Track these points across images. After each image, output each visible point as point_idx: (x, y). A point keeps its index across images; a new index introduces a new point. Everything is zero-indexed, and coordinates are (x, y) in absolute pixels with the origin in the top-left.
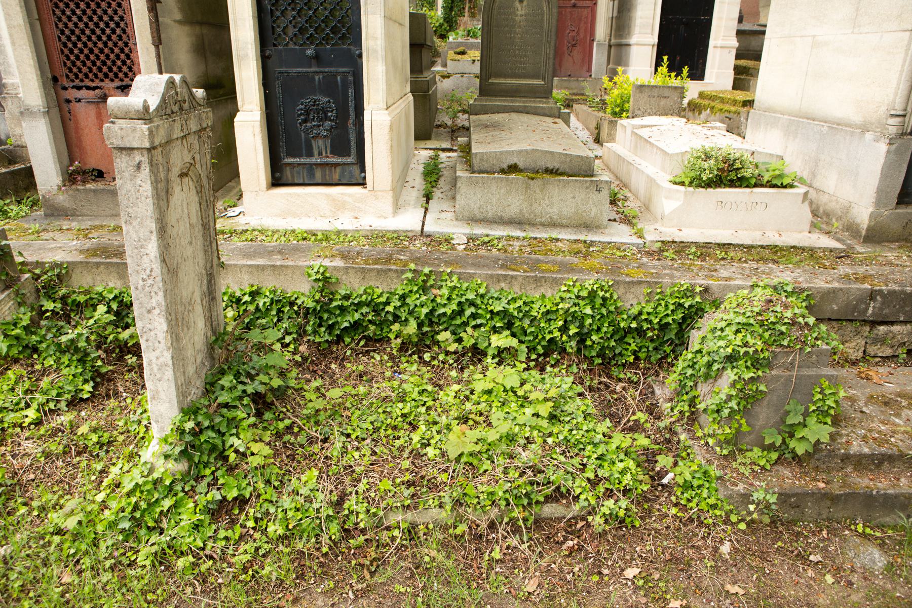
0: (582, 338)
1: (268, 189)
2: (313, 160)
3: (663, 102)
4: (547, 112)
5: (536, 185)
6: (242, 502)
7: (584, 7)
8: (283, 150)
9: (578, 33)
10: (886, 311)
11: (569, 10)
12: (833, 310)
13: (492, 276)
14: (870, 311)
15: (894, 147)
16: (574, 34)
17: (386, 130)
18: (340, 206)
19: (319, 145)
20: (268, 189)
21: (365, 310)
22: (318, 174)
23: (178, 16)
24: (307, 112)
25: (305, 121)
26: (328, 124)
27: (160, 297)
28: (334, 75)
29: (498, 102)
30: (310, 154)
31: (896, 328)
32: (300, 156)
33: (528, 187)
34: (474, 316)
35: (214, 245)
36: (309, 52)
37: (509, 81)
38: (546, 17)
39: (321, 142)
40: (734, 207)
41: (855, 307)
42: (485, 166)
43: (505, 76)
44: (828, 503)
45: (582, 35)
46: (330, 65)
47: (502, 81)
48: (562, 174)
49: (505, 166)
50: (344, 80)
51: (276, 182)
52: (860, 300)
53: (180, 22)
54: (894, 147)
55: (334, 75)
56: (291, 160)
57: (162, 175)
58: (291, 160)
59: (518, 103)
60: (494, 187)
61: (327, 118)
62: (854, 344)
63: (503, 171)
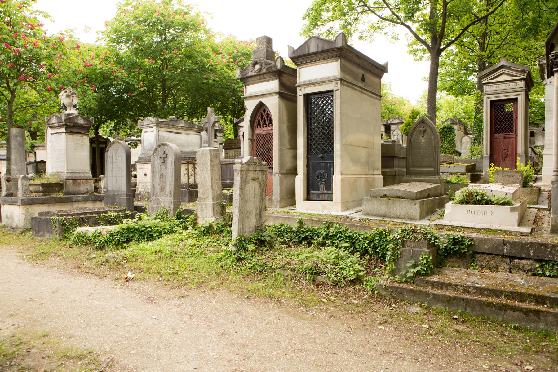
0: (375, 247)
1: (304, 200)
2: (319, 192)
3: (511, 179)
4: (435, 181)
5: (391, 201)
6: (244, 259)
7: (511, 138)
8: (310, 188)
9: (508, 151)
10: (514, 251)
11: (501, 140)
12: (486, 249)
13: (350, 225)
14: (505, 250)
15: (555, 186)
16: (506, 151)
17: (340, 181)
18: (324, 208)
19: (322, 186)
20: (304, 200)
21: (309, 232)
22: (321, 196)
23: (288, 147)
24: (319, 175)
25: (318, 178)
26: (324, 179)
27: (238, 204)
28: (327, 163)
29: (413, 178)
30: (319, 190)
31: (524, 262)
32: (315, 190)
33: (388, 203)
34: (340, 237)
35: (264, 202)
36: (319, 156)
37: (419, 169)
38: (433, 142)
39: (322, 185)
40: (476, 213)
41: (497, 249)
42: (375, 195)
43: (417, 167)
44: (412, 294)
45: (510, 152)
46: (326, 160)
47: (416, 169)
48: (403, 198)
49: (382, 195)
50: (330, 165)
51: (308, 199)
52: (499, 245)
53: (289, 149)
54: (555, 186)
55: (327, 163)
56: (313, 192)
57: (244, 177)
58: (313, 192)
59: (422, 178)
60: (375, 202)
61: (324, 178)
62: (503, 267)
63: (381, 197)
